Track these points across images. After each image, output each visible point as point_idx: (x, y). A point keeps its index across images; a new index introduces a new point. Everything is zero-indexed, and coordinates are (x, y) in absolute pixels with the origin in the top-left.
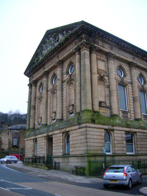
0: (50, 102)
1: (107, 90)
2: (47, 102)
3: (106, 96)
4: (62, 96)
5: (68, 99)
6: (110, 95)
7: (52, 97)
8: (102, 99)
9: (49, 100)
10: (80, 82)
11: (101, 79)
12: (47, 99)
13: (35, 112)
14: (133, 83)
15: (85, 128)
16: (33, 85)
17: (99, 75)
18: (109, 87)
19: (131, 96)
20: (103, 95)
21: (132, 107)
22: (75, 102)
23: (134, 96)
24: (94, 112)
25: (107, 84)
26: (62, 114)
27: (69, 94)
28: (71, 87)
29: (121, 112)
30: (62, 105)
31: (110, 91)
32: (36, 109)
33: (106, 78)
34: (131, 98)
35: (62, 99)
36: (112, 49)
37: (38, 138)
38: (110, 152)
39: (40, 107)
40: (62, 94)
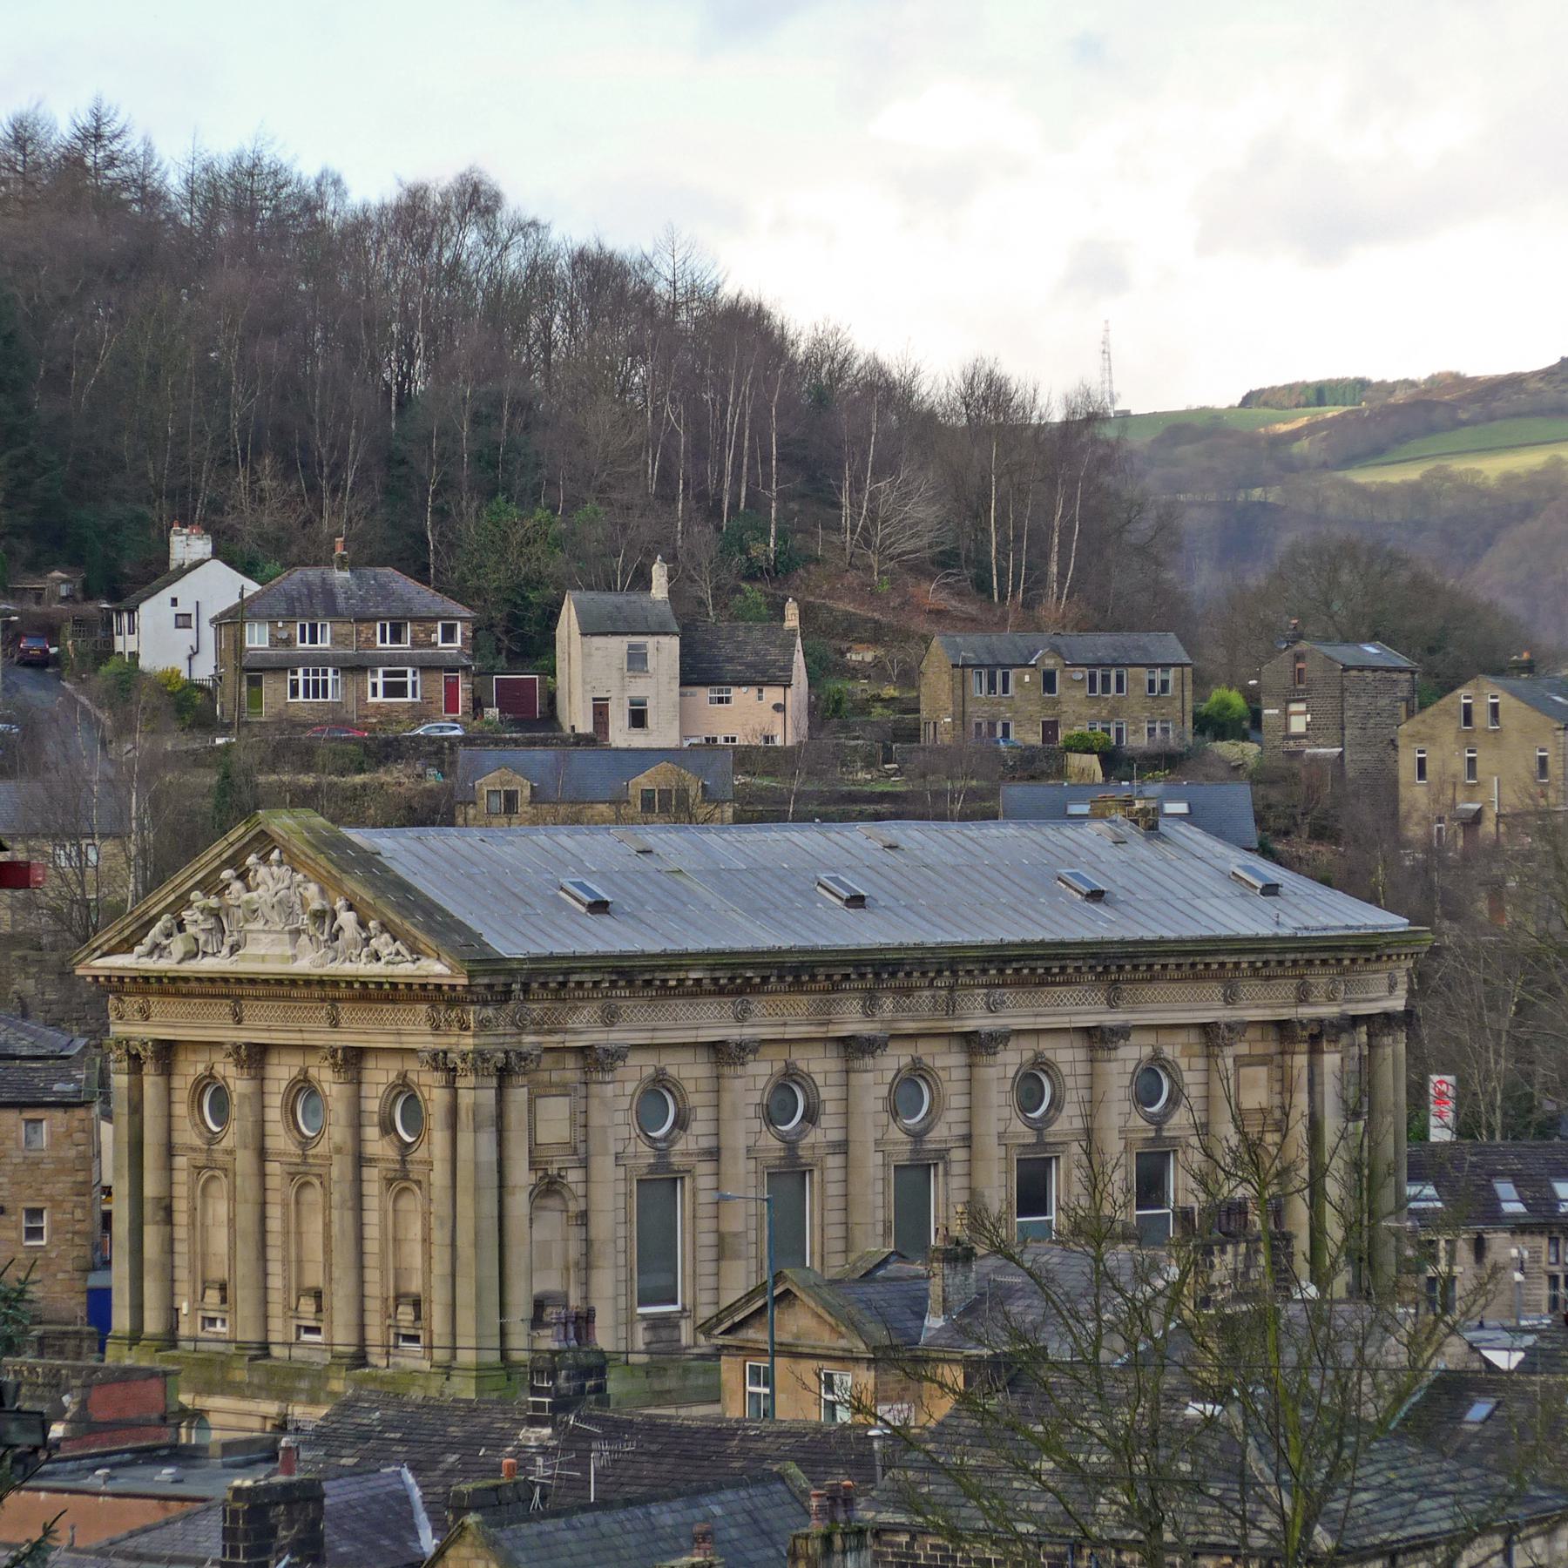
0: (286, 1233)
1: (576, 1233)
2: (263, 1218)
3: (567, 1269)
4: (360, 1238)
5: (391, 1265)
6: (586, 1265)
7: (298, 1202)
8: (549, 1282)
9: (274, 1212)
10: (450, 1224)
11: (548, 1187)
12: (263, 1204)
13: (172, 1240)
14: (725, 1155)
15: (446, 1342)
16: (149, 1068)
17: (540, 1174)
18: (584, 1218)
19: (706, 1224)
20: (557, 1262)
21: (709, 1282)
22: (427, 1284)
23: (726, 1227)
24: (505, 538)
25: (574, 1207)
26: (362, 1327)
27: (395, 1240)
28: (406, 1203)
29: (640, 1328)
30: (361, 1282)
31: (588, 1242)
32: (181, 1218)
33: (573, 1176)
34: (708, 1239)
35: (360, 1253)
36: (610, 1018)
37: (217, 1411)
38: (675, 1303)
39: (204, 1214)
40: (360, 1225)
